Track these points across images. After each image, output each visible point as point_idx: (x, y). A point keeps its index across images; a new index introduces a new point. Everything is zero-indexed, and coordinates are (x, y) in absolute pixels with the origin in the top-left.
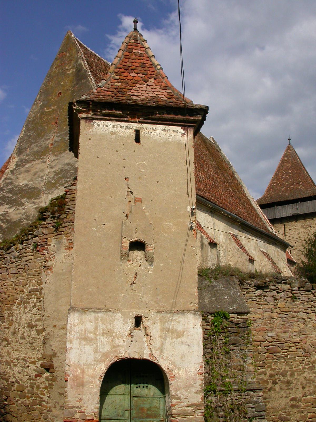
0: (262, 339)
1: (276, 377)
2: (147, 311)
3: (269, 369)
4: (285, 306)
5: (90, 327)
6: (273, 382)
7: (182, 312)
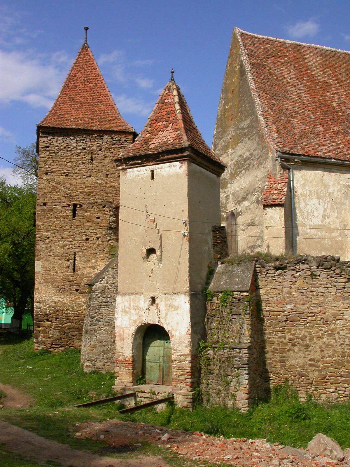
0: (281, 310)
1: (296, 340)
2: (157, 293)
3: (289, 334)
4: (303, 283)
5: (127, 304)
6: (292, 344)
7: (177, 294)
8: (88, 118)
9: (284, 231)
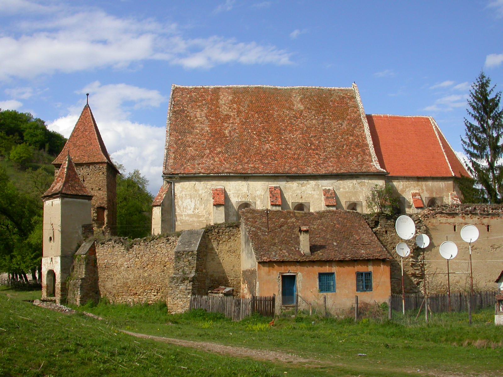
7: (57, 256)
8: (82, 156)
9: (161, 220)
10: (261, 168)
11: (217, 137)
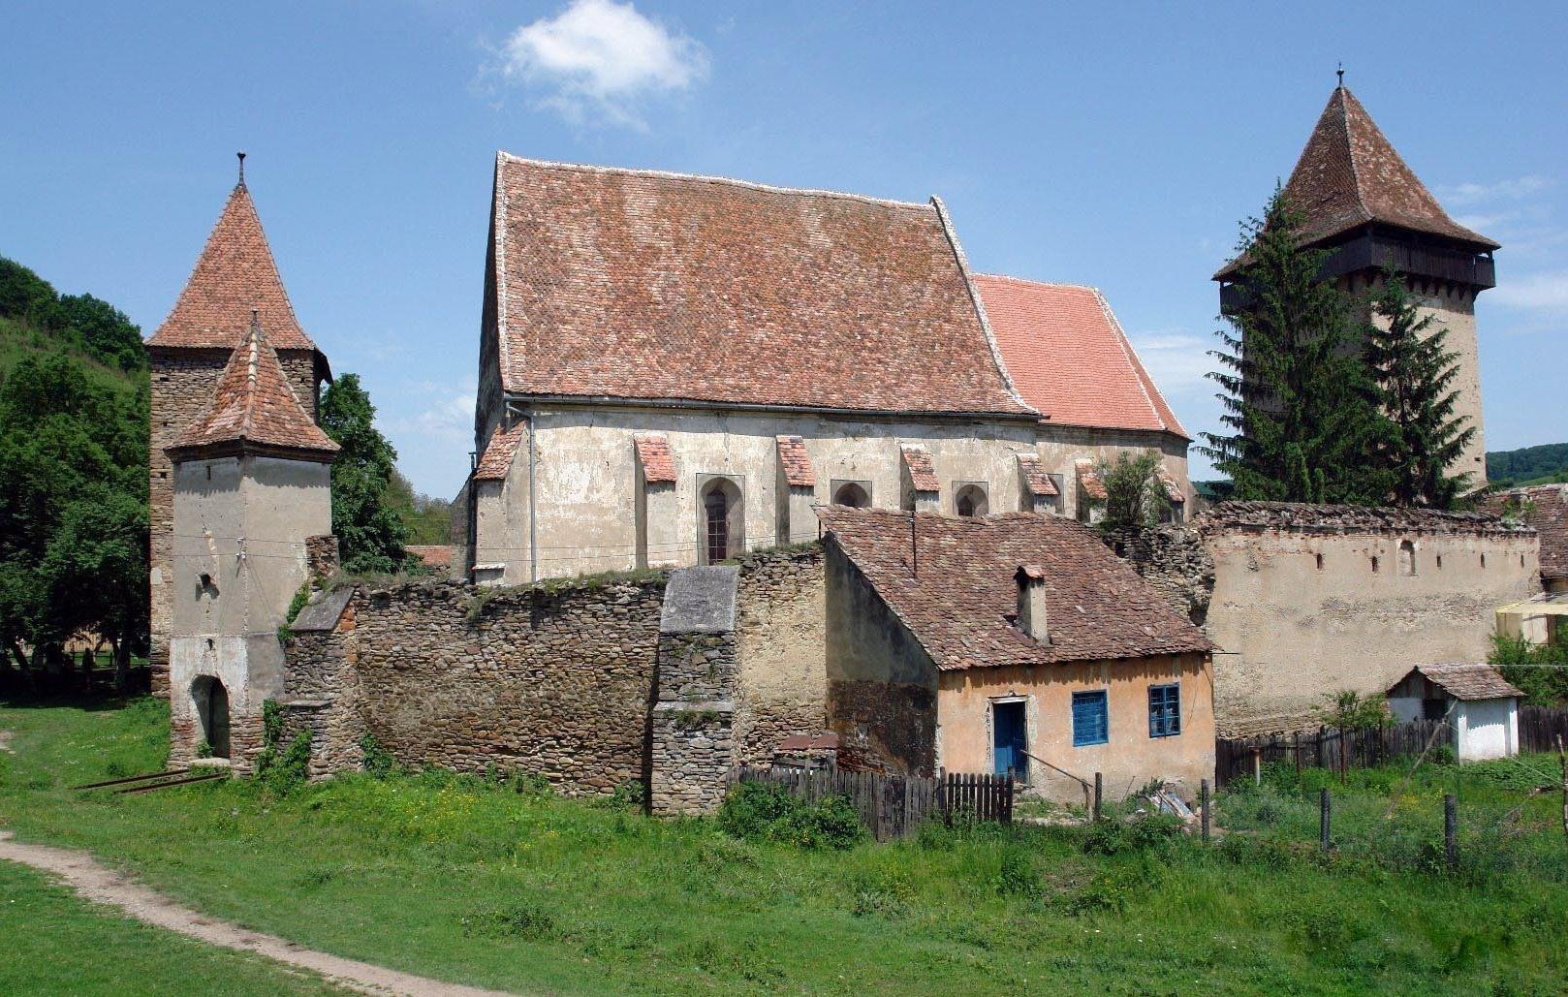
10: (757, 393)
11: (631, 303)
